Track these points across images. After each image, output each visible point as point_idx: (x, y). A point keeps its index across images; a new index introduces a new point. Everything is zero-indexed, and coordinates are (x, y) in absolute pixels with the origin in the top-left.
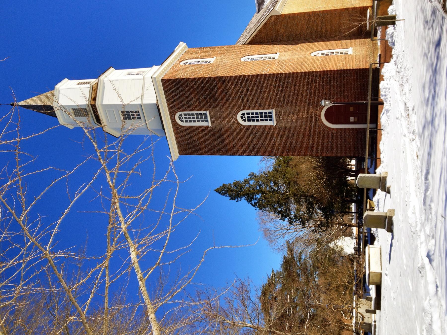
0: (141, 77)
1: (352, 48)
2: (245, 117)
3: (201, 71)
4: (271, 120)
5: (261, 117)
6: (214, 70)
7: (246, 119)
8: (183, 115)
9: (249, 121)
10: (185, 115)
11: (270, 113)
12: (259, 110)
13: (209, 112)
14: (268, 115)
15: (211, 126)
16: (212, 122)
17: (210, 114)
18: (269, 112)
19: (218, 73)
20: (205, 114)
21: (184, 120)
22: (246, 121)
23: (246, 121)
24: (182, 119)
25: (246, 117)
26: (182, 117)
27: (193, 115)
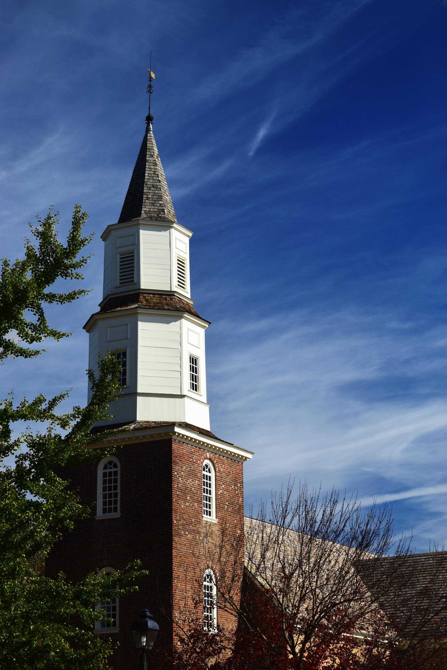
0: (186, 389)
1: (216, 522)
2: (111, 468)
3: (187, 504)
4: (104, 511)
5: (110, 495)
6: (187, 527)
7: (108, 471)
8: (115, 469)
9: (105, 475)
10: (116, 473)
11: (115, 510)
12: (119, 605)
13: (116, 633)
14: (113, 492)
15: (95, 519)
16: (102, 521)
17: (115, 520)
18: (117, 493)
19: (180, 536)
20: (115, 510)
21: (108, 471)
22: (103, 469)
23: (103, 469)
24: (109, 467)
25: (110, 470)
26: (112, 466)
27: (115, 488)
